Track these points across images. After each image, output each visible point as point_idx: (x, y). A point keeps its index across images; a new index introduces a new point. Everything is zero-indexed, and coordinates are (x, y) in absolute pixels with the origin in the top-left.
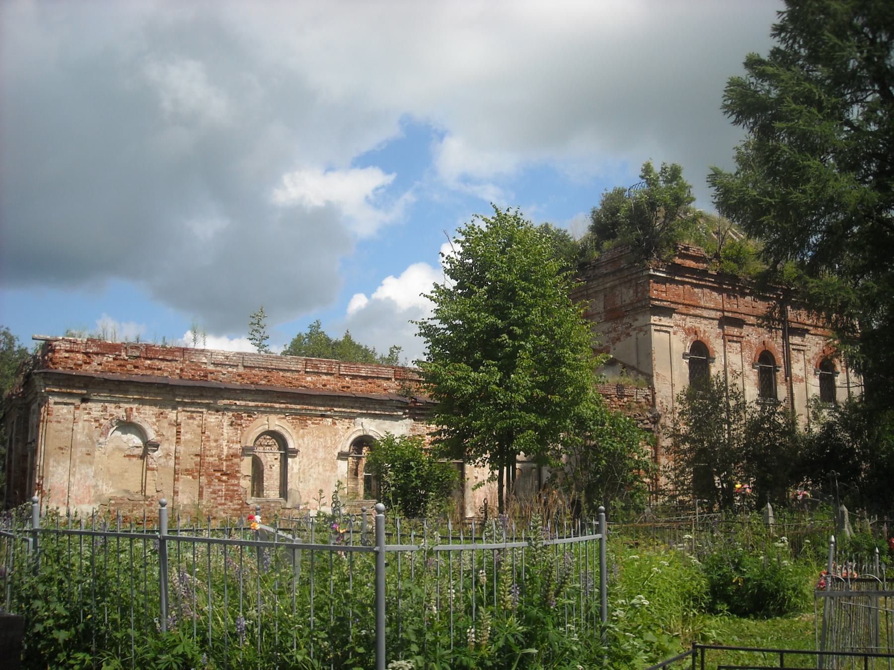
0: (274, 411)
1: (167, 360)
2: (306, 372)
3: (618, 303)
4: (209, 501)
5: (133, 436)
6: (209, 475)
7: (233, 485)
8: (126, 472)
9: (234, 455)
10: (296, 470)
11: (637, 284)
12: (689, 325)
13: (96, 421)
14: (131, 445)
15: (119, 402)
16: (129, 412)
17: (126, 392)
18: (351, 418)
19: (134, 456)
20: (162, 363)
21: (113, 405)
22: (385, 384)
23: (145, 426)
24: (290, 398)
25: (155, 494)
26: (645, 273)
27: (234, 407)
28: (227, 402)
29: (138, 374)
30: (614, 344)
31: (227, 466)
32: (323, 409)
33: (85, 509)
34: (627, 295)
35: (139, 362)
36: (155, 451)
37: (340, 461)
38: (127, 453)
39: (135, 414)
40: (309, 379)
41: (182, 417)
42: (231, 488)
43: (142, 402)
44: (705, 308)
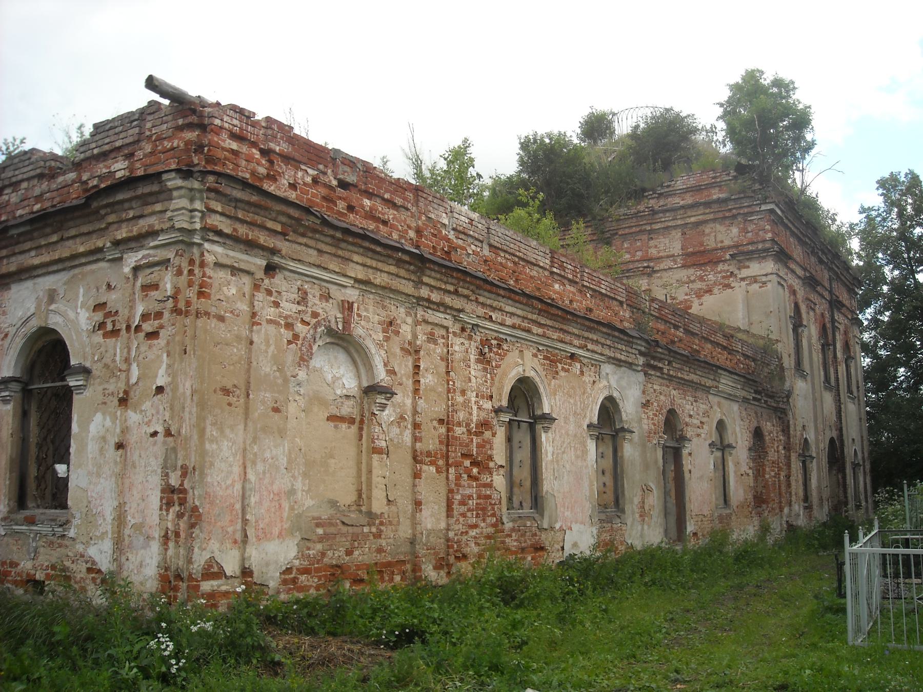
8: (332, 456)
13: (289, 326)
14: (339, 392)
25: (385, 509)
30: (699, 296)
33: (275, 556)
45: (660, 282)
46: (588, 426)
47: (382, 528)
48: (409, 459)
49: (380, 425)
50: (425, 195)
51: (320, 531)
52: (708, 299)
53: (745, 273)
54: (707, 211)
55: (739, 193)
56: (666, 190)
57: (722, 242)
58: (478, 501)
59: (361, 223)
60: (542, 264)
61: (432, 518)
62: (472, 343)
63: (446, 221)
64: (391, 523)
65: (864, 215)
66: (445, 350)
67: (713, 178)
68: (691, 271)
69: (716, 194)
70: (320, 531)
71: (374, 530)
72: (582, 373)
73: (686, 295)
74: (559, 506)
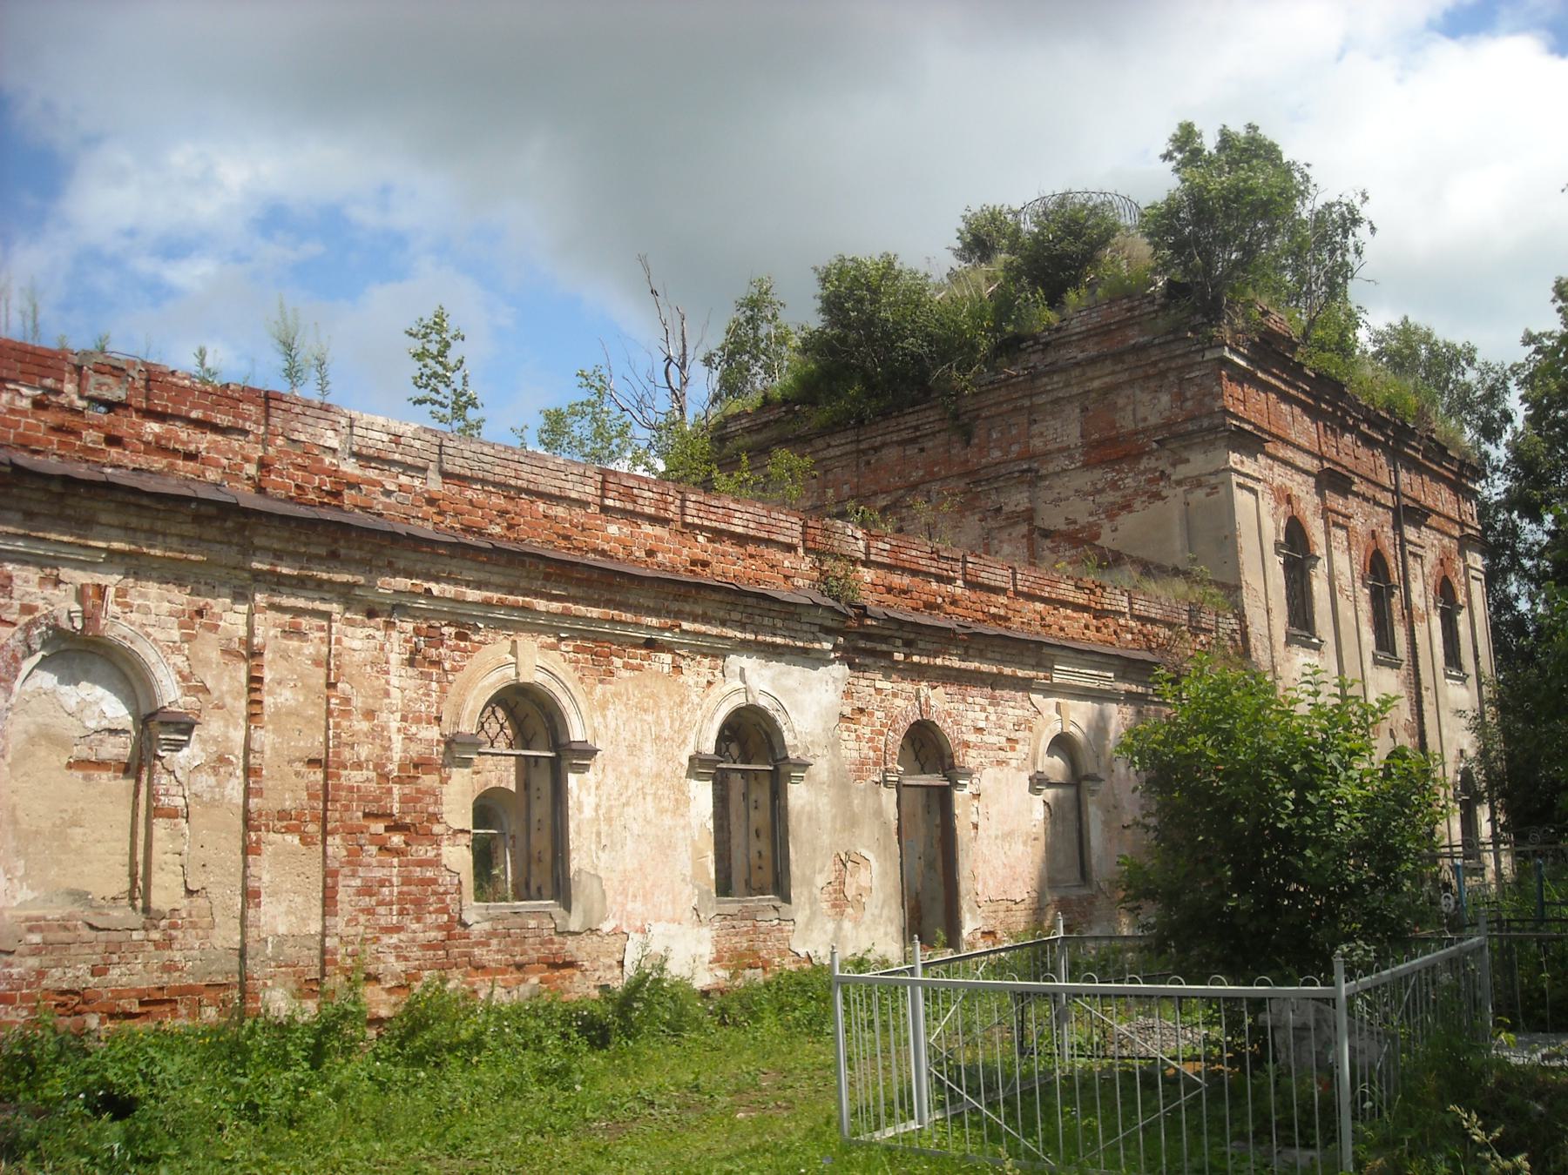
0: (528, 622)
1: (216, 429)
2: (605, 509)
3: (1126, 423)
4: (353, 921)
5: (99, 691)
6: (352, 832)
7: (421, 864)
8: (76, 824)
9: (422, 764)
10: (588, 812)
11: (1181, 380)
12: (1278, 481)
14: (92, 724)
15: (56, 562)
16: (92, 597)
17: (85, 524)
18: (715, 656)
19: (101, 765)
20: (197, 435)
21: (33, 574)
22: (787, 561)
23: (149, 654)
24: (579, 583)
25: (183, 903)
26: (1208, 355)
27: (422, 603)
28: (402, 583)
29: (120, 465)
30: (1111, 516)
31: (404, 800)
32: (654, 622)
34: (1151, 407)
35: (124, 425)
36: (178, 746)
37: (693, 783)
38: (81, 751)
39: (113, 609)
40: (613, 529)
41: (267, 628)
42: (417, 872)
43: (136, 566)
44: (1299, 448)
45: (1050, 496)
46: (691, 759)
47: (174, 933)
48: (239, 822)
49: (172, 772)
50: (284, 406)
51: (36, 938)
52: (1126, 520)
53: (1182, 471)
54: (1119, 367)
55: (1168, 333)
56: (1056, 336)
57: (1145, 419)
58: (405, 889)
59: (133, 461)
60: (574, 495)
61: (287, 914)
62: (394, 634)
63: (333, 442)
64: (194, 925)
65: (1533, 347)
66: (325, 649)
67: (1129, 310)
68: (1097, 474)
69: (1135, 337)
70: (36, 938)
71: (155, 935)
72: (677, 669)
73: (1091, 514)
74: (610, 894)
